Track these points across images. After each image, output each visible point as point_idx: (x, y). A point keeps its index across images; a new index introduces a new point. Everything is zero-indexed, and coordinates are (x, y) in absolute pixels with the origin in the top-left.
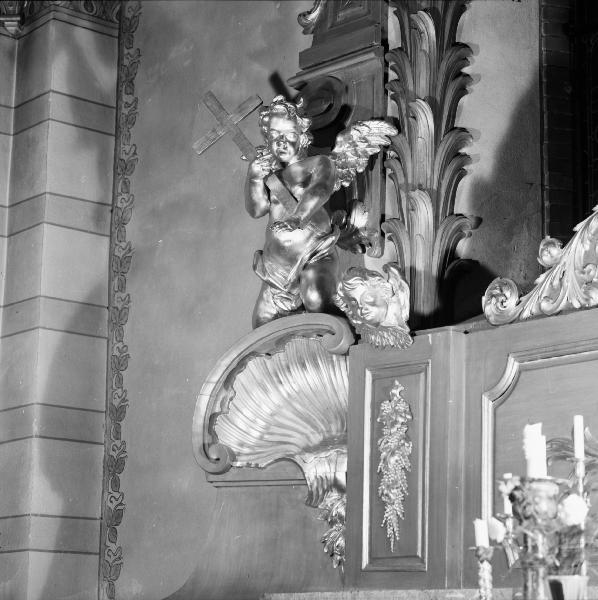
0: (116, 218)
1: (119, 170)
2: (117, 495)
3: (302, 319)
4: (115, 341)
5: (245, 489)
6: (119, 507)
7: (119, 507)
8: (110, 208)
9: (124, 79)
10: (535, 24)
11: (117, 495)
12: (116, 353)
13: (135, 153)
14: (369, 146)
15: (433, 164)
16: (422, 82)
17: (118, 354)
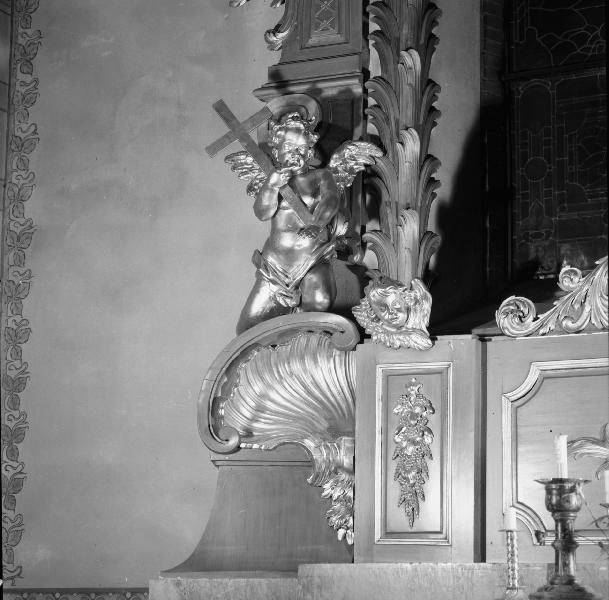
0: (11, 194)
1: (13, 147)
2: (15, 464)
3: (299, 318)
4: (10, 314)
5: (255, 469)
6: (19, 476)
7: (19, 476)
8: (3, 183)
9: (18, 57)
10: (477, 69)
11: (15, 464)
12: (11, 324)
13: (35, 132)
14: (356, 164)
15: (418, 184)
16: (405, 109)
17: (15, 327)
